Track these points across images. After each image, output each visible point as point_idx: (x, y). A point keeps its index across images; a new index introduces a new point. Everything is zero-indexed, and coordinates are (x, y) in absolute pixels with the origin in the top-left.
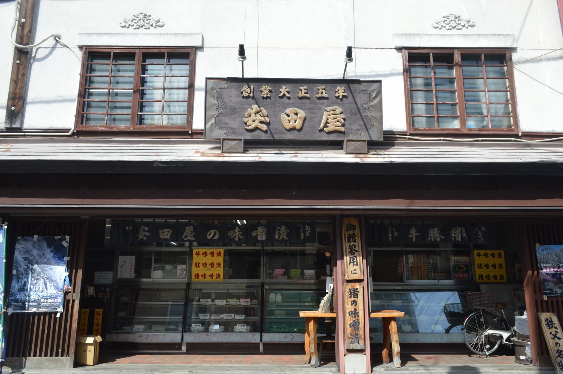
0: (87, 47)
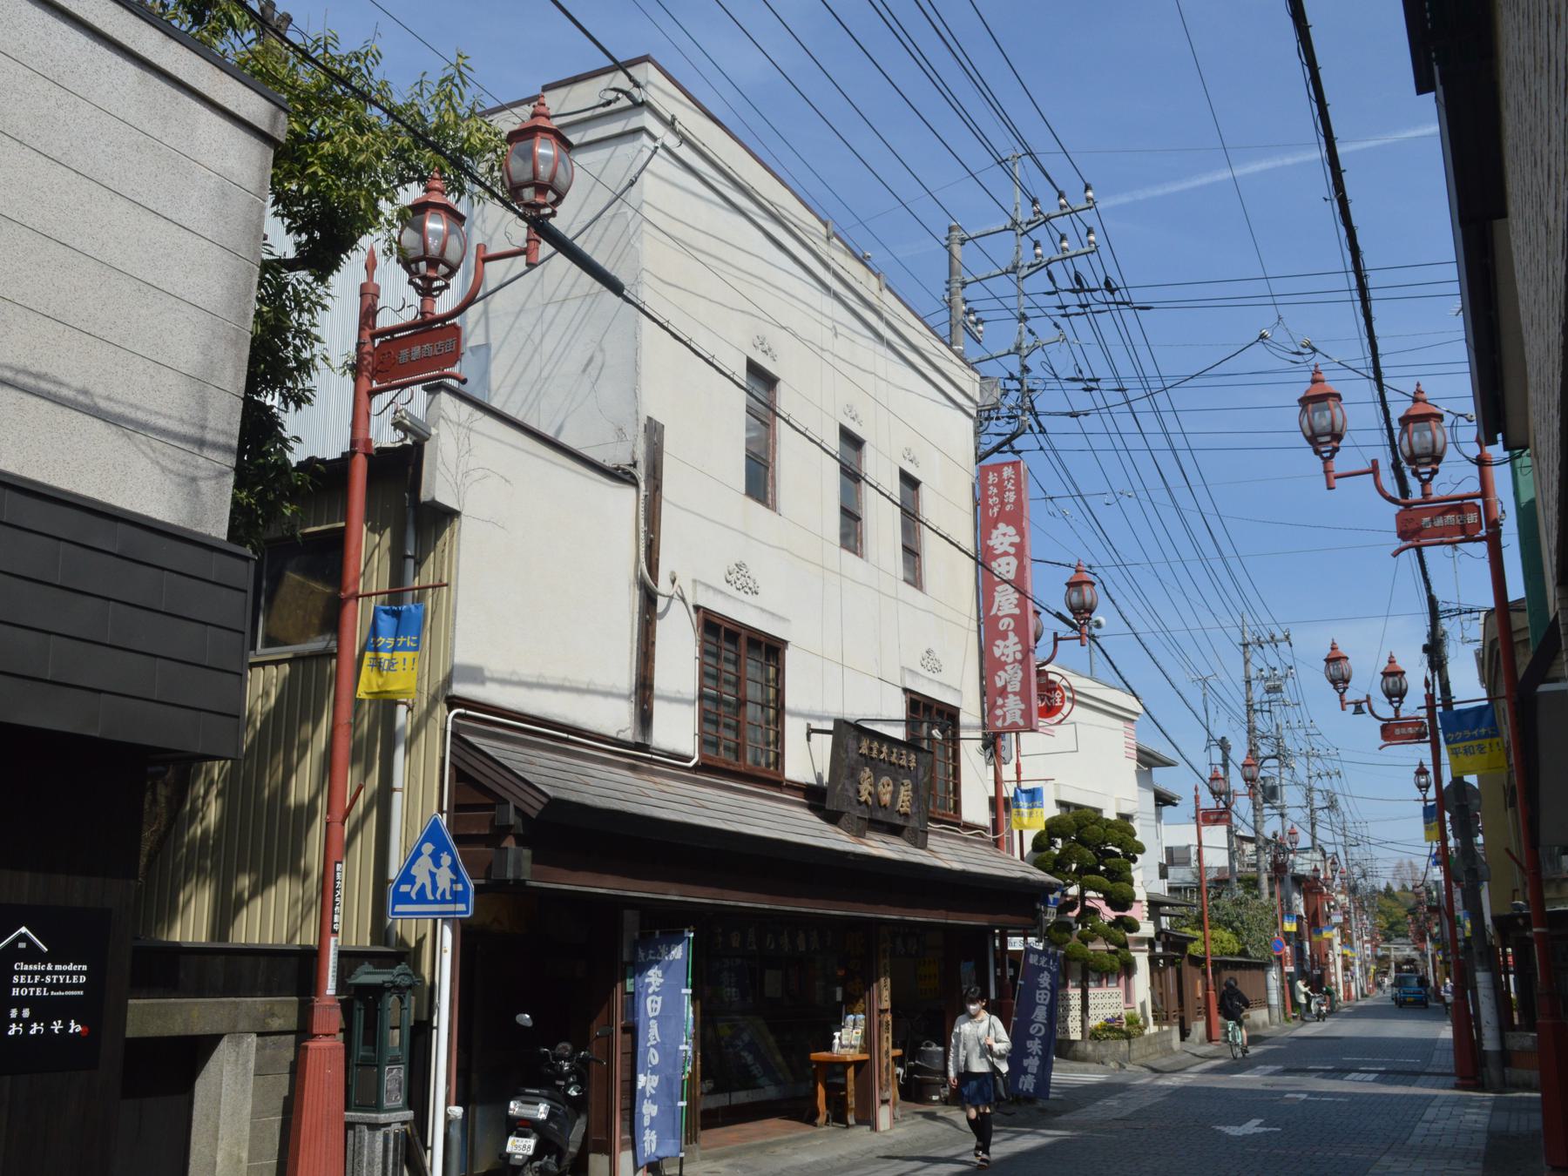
0: (707, 611)
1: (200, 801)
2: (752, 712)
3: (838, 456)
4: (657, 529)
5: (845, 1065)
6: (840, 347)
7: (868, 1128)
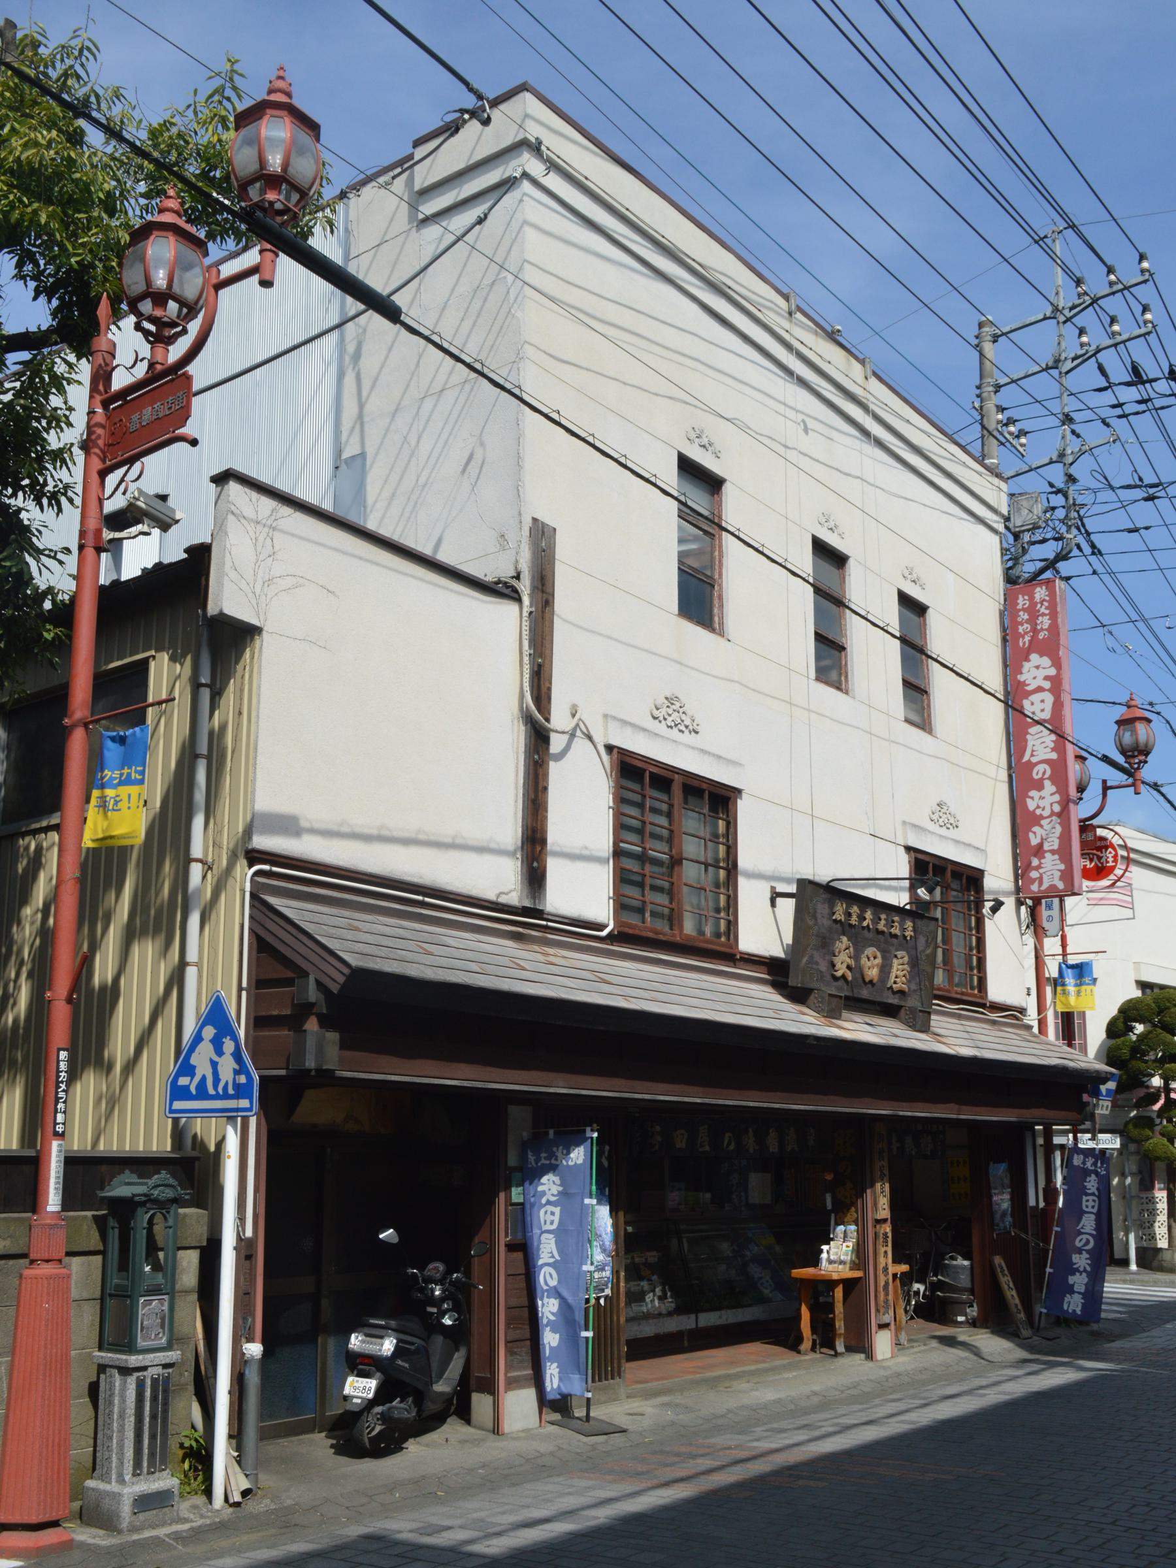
0: (623, 752)
1: (12, 984)
2: (690, 872)
3: (811, 580)
4: (547, 652)
5: (831, 1284)
6: (806, 443)
7: (863, 1356)
